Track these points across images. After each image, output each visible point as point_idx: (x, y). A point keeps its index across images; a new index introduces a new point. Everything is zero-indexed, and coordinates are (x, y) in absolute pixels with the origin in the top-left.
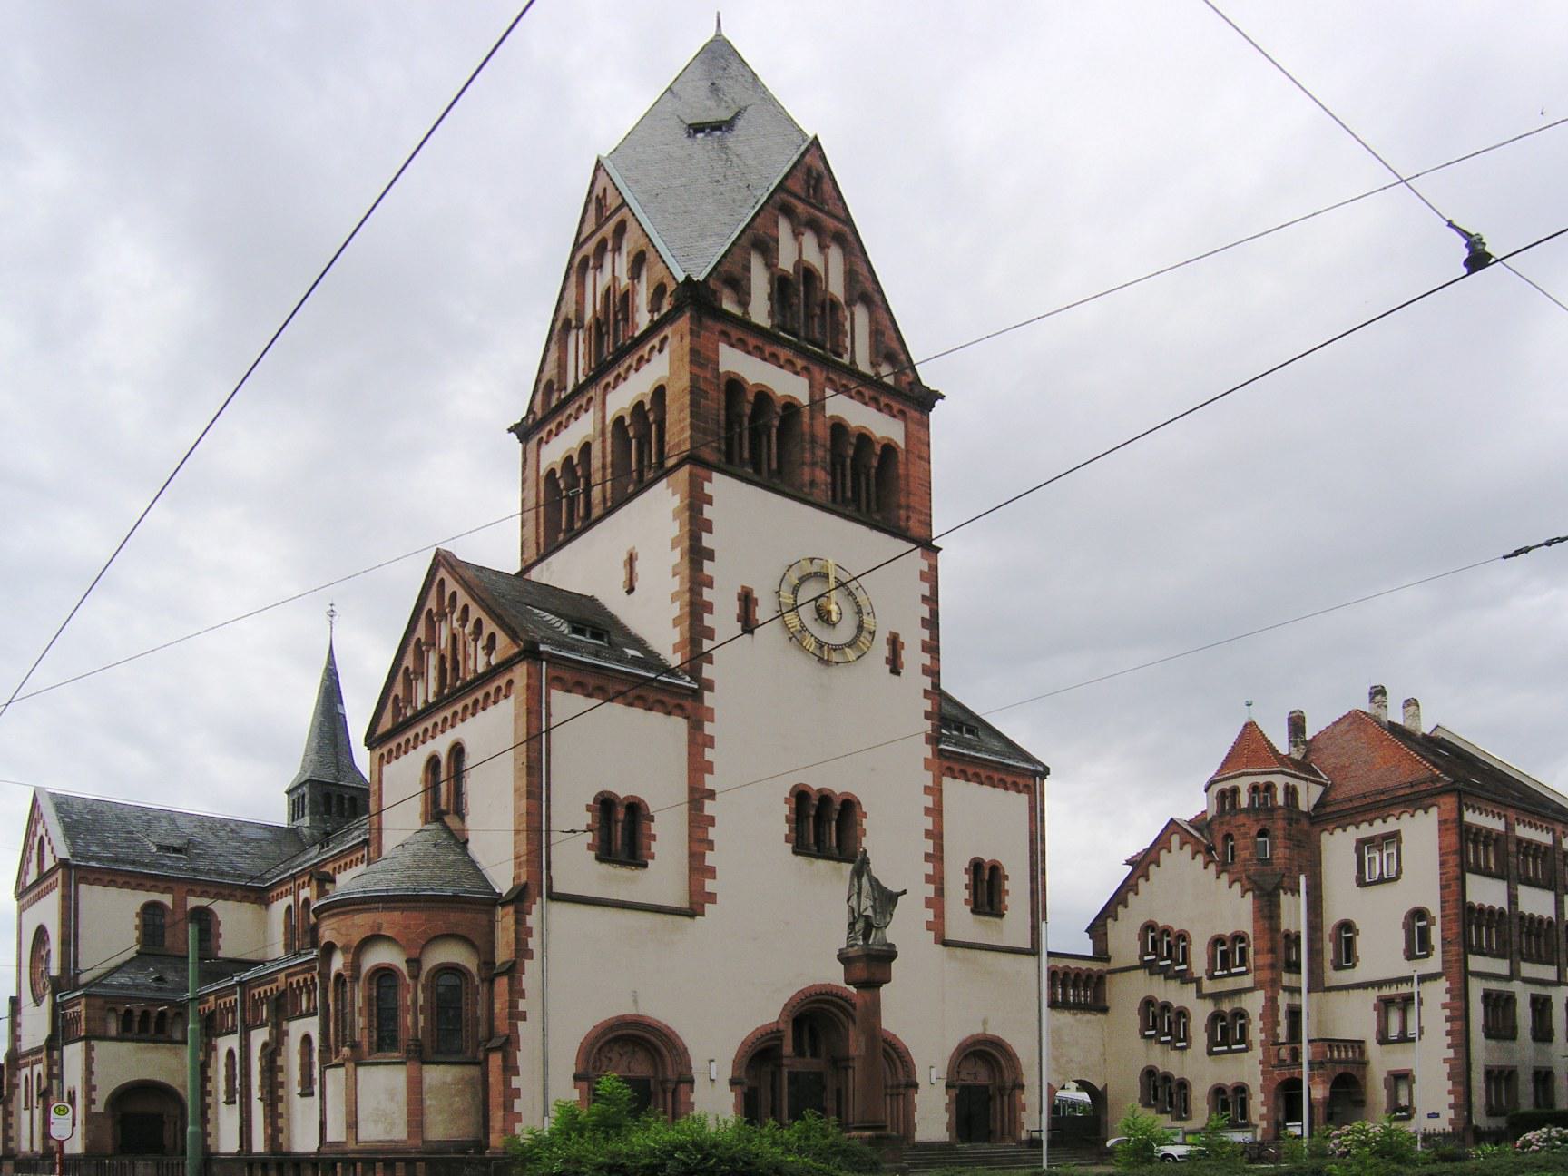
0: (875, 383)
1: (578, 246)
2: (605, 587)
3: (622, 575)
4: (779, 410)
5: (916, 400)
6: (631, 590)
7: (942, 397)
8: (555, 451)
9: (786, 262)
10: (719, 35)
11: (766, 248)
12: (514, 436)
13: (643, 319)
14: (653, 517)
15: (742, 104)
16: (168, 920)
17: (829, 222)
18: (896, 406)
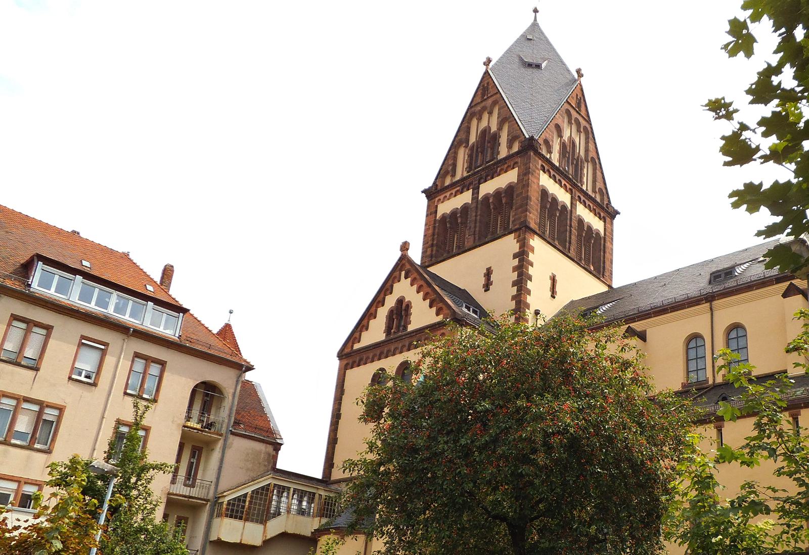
0: (593, 200)
1: (470, 107)
2: (473, 285)
3: (482, 281)
4: (559, 208)
5: (608, 213)
6: (553, 280)
7: (619, 213)
10: (535, 25)
12: (424, 195)
15: (757, 144)
17: (583, 123)
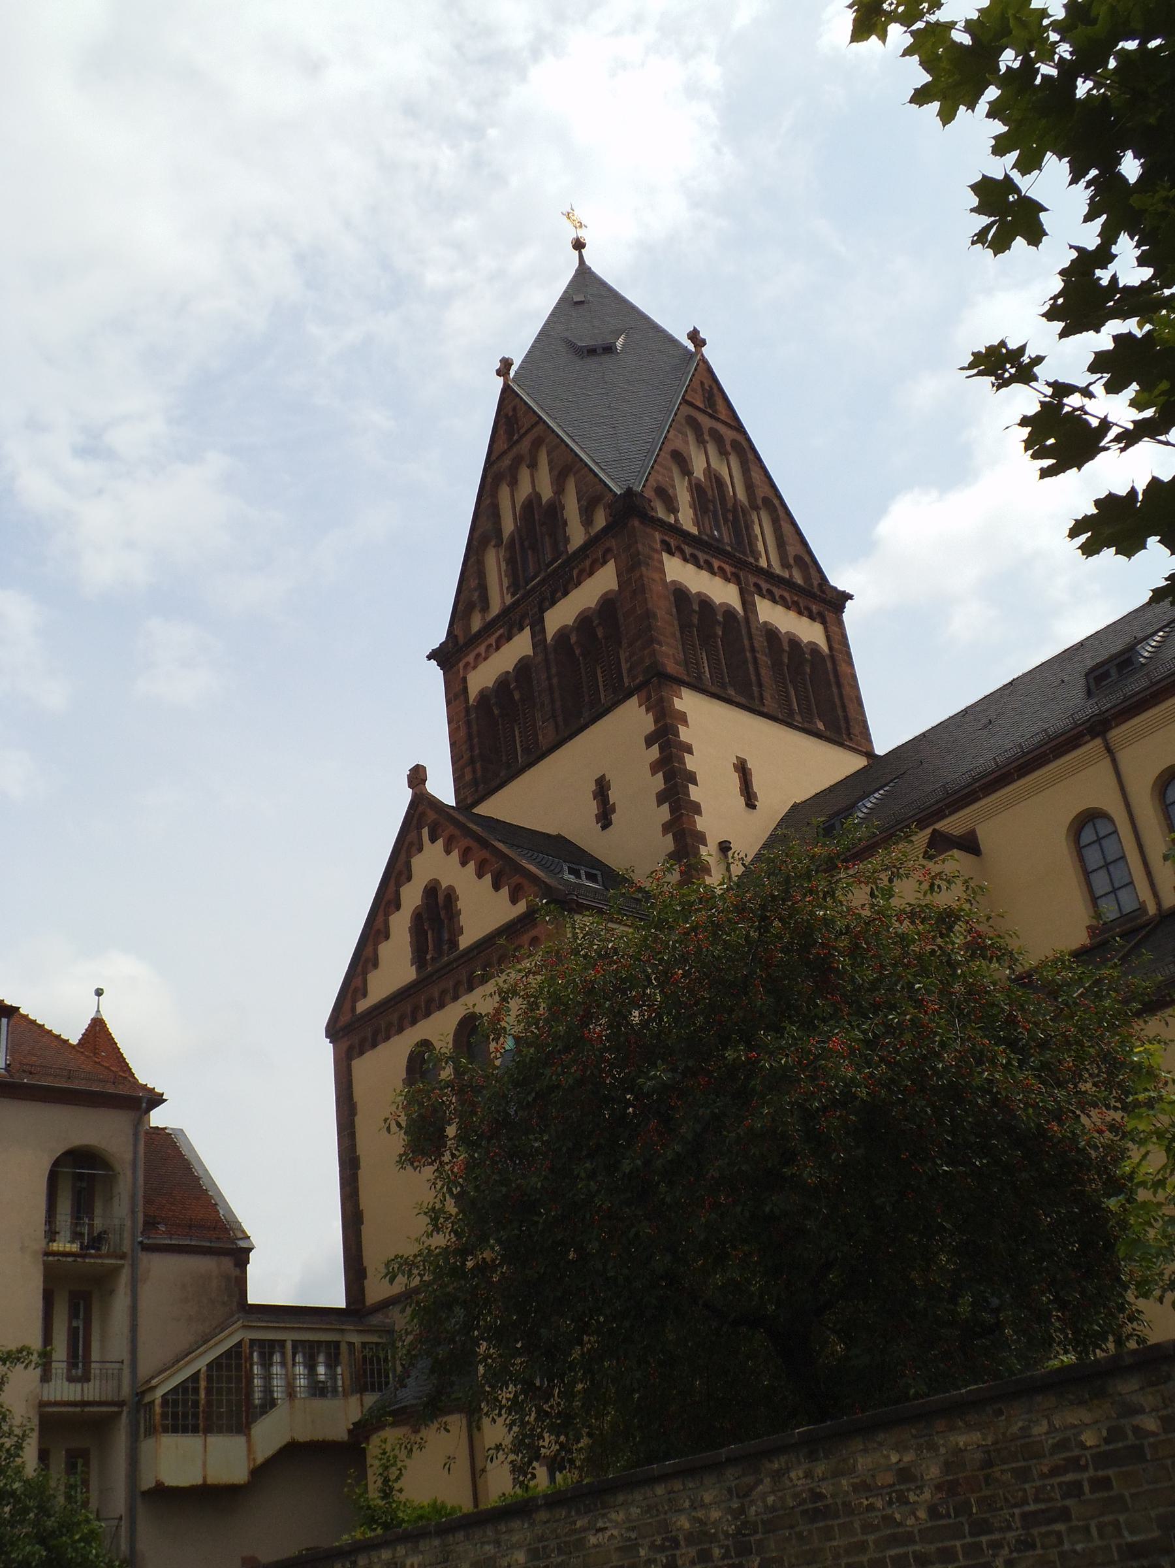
0: (789, 584)
3: (593, 807)
5: (829, 604)
7: (850, 597)
8: (481, 678)
9: (699, 467)
11: (682, 462)
12: (433, 663)
13: (577, 536)
14: (617, 740)
16: (1146, 1063)
18: (702, 557)
